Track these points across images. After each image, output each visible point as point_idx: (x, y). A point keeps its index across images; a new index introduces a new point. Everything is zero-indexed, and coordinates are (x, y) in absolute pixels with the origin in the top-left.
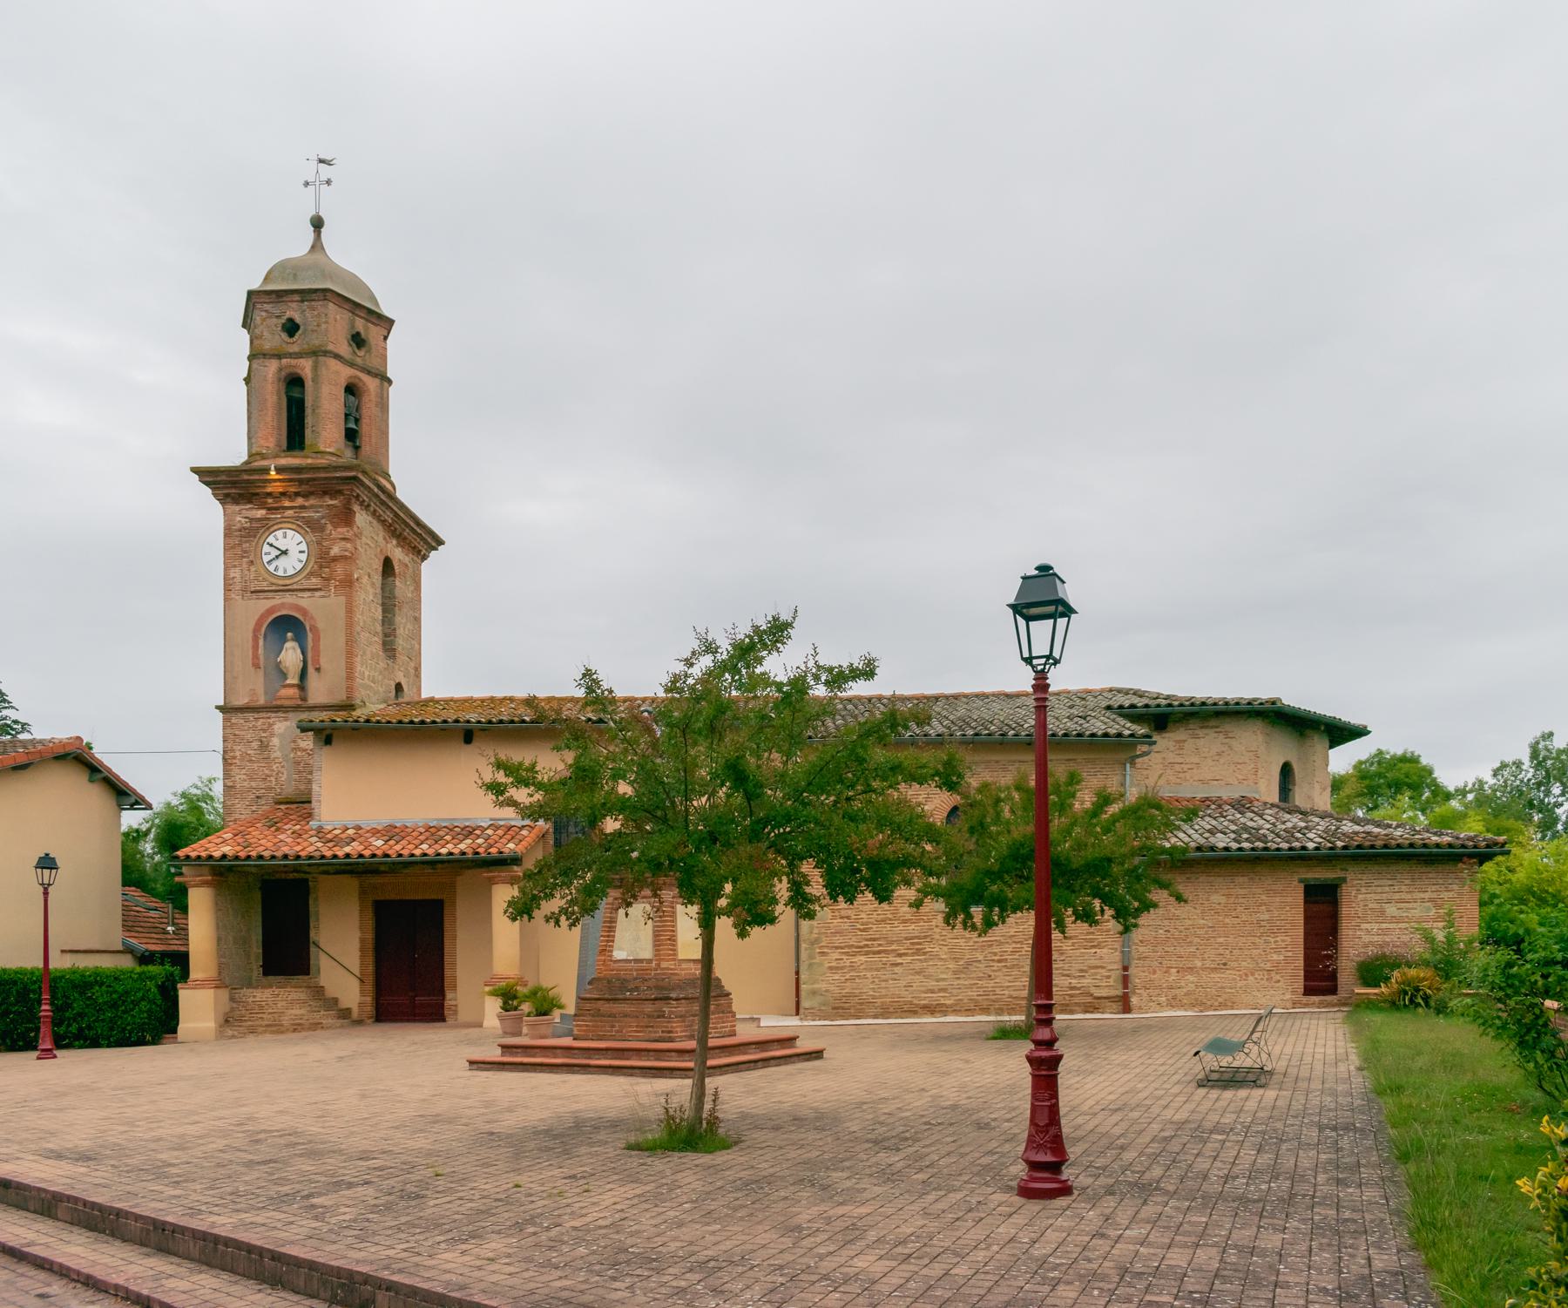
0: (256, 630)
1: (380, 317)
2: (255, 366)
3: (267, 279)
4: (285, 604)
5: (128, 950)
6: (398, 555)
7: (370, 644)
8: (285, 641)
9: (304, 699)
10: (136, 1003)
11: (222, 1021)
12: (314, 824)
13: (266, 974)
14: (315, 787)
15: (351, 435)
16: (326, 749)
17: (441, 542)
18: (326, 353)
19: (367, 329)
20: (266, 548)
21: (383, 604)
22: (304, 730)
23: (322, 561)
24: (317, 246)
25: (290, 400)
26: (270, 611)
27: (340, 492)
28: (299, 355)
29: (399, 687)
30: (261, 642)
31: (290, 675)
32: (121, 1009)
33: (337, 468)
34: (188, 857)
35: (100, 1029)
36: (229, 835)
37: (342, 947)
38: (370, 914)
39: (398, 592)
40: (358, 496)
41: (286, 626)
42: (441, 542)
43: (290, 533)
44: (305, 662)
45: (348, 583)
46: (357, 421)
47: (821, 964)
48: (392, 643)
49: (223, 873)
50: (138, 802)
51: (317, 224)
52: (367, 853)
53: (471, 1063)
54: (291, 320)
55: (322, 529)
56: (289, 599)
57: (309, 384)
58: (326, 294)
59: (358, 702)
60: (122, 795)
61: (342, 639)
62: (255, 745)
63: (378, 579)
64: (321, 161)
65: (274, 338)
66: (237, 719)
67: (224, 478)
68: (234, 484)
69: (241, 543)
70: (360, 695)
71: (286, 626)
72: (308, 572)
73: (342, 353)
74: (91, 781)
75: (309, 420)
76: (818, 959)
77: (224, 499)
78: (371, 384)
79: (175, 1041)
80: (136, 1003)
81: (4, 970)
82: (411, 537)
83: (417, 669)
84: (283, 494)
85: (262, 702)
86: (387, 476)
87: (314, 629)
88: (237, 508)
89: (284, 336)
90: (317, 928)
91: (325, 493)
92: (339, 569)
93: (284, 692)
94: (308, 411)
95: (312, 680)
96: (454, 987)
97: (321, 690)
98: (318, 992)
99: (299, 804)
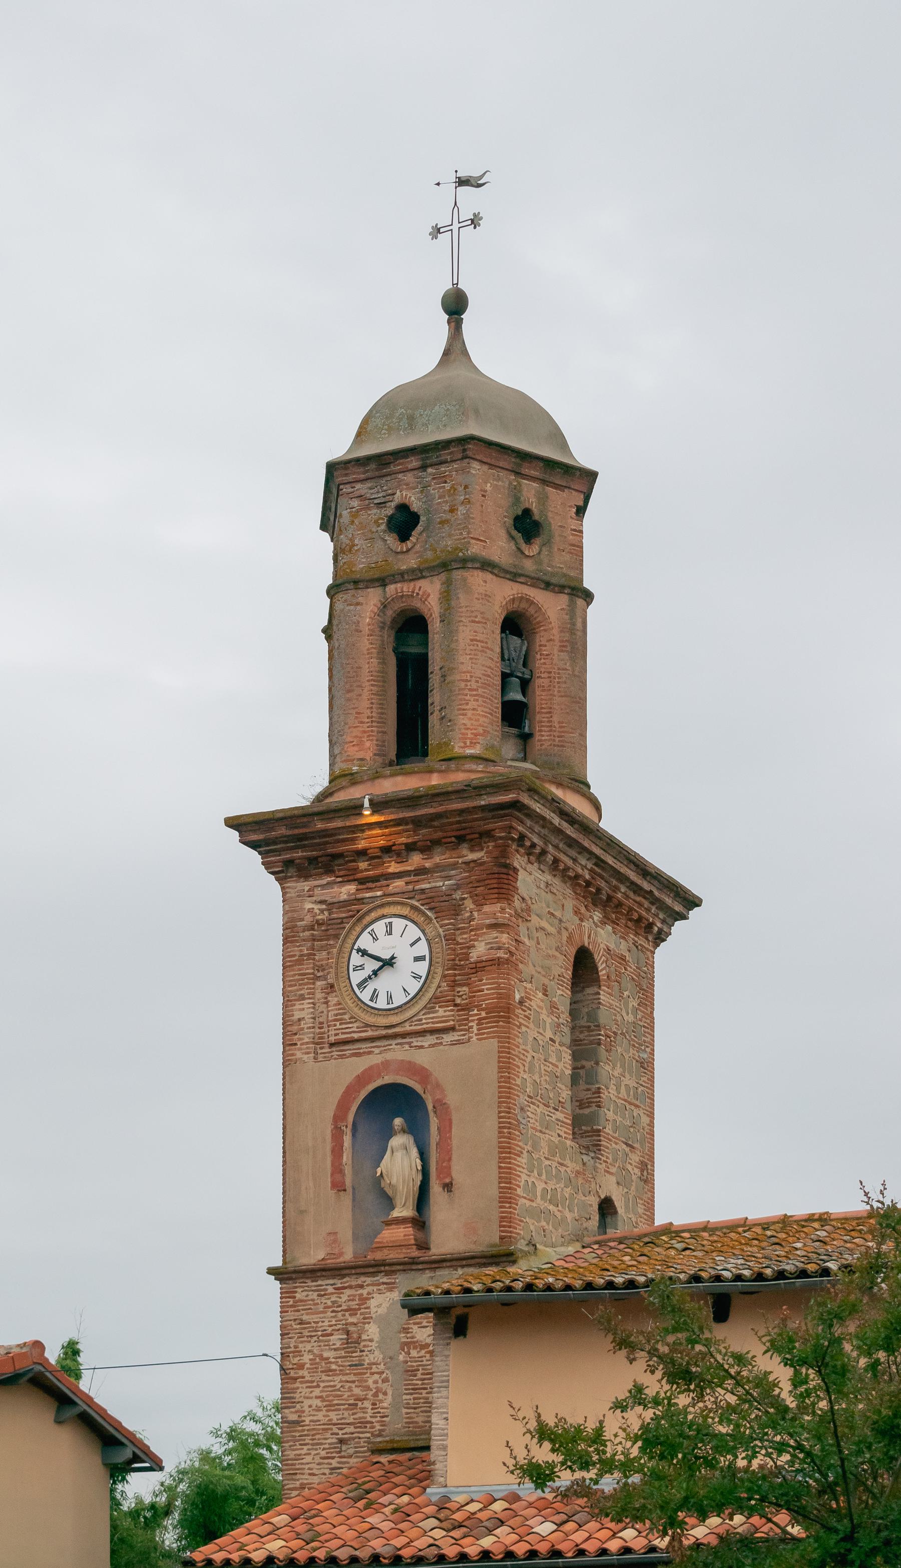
0: (339, 1117)
2: (339, 606)
3: (362, 434)
4: (388, 1062)
6: (604, 938)
7: (546, 1127)
8: (389, 1133)
9: (423, 1246)
12: (434, 1492)
14: (436, 1420)
15: (514, 715)
16: (457, 1344)
17: (692, 902)
18: (465, 563)
20: (356, 959)
21: (575, 1042)
22: (414, 1311)
23: (457, 973)
24: (455, 350)
26: (361, 1080)
27: (488, 834)
28: (417, 574)
29: (606, 1208)
30: (347, 1140)
31: (399, 1201)
33: (479, 789)
36: (281, 1520)
39: (603, 1016)
40: (522, 837)
41: (393, 1105)
42: (692, 902)
43: (399, 924)
44: (425, 1172)
45: (503, 1012)
46: (525, 684)
48: (592, 1119)
50: (142, 1458)
51: (455, 305)
52: (521, 1549)
54: (403, 508)
55: (456, 910)
56: (397, 1052)
57: (435, 626)
58: (465, 446)
59: (522, 1245)
60: (115, 1448)
61: (491, 1124)
62: (337, 1339)
63: (562, 995)
64: (462, 182)
65: (376, 548)
66: (304, 1292)
67: (282, 831)
68: (300, 840)
69: (313, 951)
70: (528, 1227)
71: (393, 1105)
72: (430, 997)
73: (495, 558)
74: (58, 1422)
75: (435, 698)
77: (284, 870)
78: (551, 606)
82: (630, 900)
85: (348, 1256)
86: (581, 785)
87: (442, 1107)
88: (305, 885)
89: (392, 540)
91: (461, 839)
92: (487, 986)
94: (434, 680)
97: (450, 1231)
99: (409, 1452)
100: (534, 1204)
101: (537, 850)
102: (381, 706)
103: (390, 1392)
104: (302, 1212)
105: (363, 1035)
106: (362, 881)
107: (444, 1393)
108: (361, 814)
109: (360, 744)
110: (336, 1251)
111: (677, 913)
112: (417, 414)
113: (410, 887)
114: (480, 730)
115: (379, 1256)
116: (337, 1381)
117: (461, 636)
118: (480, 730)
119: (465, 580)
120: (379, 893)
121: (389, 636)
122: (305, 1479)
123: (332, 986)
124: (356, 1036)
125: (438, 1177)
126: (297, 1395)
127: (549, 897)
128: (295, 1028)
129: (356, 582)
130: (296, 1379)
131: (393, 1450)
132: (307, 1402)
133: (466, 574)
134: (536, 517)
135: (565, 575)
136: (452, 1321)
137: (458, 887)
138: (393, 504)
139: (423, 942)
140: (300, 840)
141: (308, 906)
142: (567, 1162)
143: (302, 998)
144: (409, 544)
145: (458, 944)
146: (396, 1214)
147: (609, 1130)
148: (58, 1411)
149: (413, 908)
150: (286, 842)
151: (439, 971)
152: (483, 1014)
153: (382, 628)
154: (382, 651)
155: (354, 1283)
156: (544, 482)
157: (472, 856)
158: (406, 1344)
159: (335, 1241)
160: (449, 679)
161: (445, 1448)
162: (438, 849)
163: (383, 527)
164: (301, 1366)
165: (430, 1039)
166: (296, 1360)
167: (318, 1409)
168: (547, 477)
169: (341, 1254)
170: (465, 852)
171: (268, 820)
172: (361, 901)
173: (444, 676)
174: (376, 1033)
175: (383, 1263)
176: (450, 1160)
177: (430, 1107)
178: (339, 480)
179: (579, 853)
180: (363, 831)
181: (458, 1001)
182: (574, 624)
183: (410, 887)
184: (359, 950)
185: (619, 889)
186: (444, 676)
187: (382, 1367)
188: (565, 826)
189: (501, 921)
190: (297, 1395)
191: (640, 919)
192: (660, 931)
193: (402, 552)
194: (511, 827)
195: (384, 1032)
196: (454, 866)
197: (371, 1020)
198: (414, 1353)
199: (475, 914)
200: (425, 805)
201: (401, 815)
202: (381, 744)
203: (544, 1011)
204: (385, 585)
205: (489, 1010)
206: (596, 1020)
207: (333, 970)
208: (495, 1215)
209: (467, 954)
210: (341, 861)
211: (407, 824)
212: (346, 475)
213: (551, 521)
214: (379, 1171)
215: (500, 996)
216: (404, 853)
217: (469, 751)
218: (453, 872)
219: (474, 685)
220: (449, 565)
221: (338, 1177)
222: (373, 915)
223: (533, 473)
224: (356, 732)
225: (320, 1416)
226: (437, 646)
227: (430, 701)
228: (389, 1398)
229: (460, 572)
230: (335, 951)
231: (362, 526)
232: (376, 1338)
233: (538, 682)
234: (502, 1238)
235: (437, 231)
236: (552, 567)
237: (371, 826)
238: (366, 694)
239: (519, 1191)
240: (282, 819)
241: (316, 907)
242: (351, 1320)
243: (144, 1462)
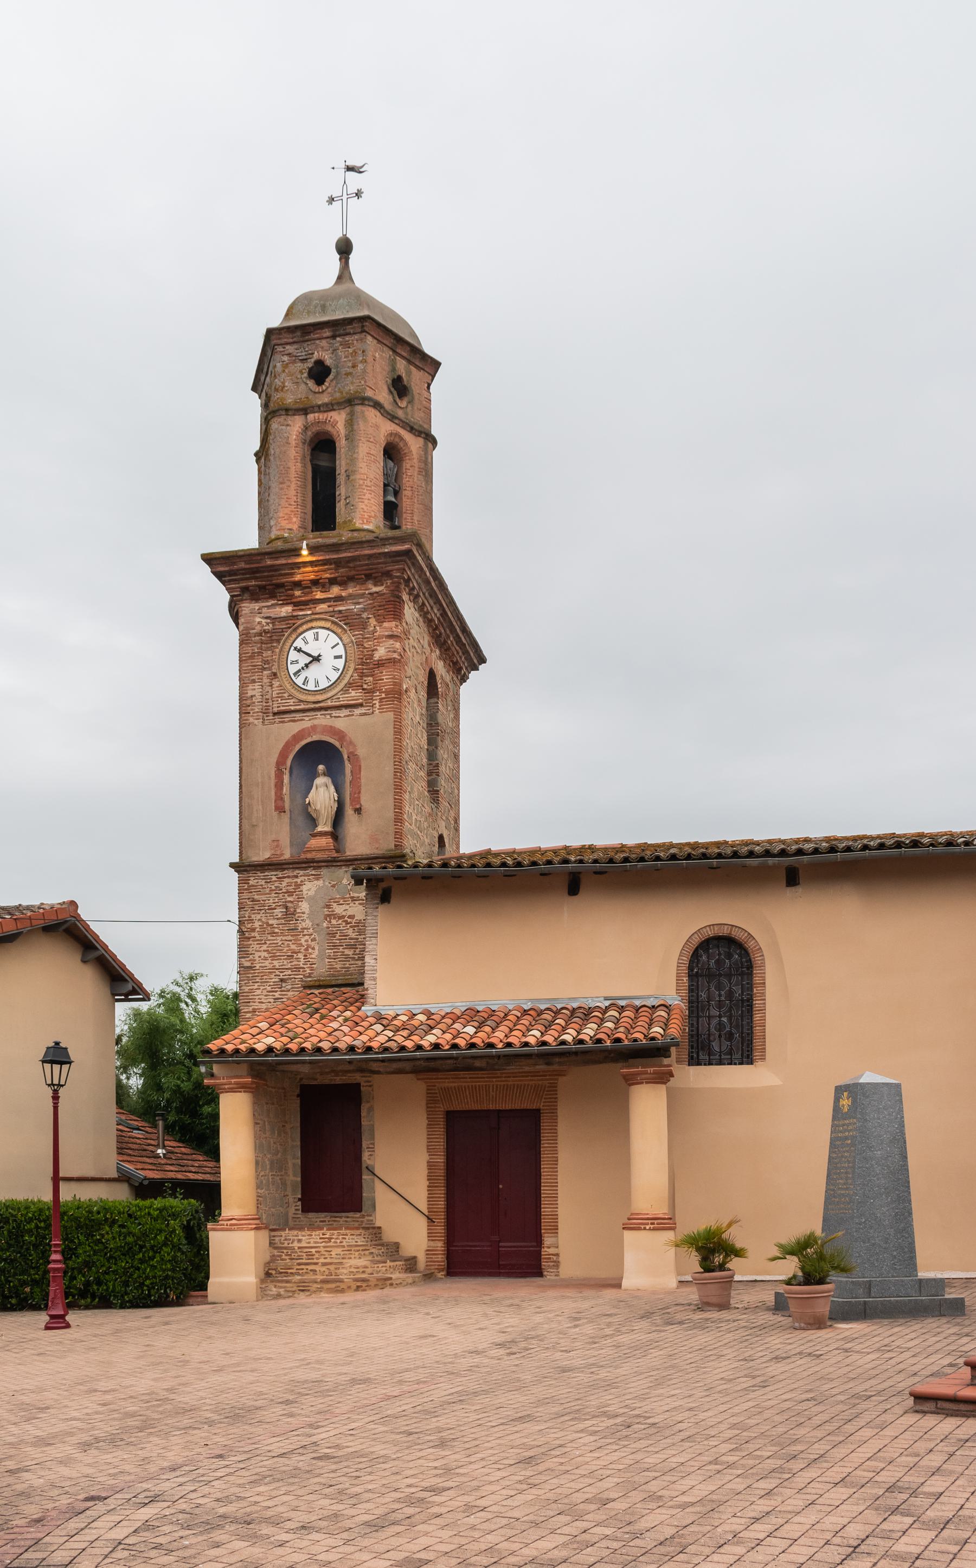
0: (280, 763)
1: (424, 357)
4: (316, 726)
5: (123, 1177)
8: (315, 775)
10: (156, 1249)
11: (262, 1275)
12: (367, 1009)
13: (306, 1209)
18: (364, 400)
19: (409, 373)
20: (293, 655)
23: (364, 668)
24: (344, 275)
25: (316, 471)
26: (297, 737)
27: (388, 574)
30: (286, 778)
32: (119, 1255)
34: (222, 1051)
35: (114, 1283)
36: (264, 1025)
37: (403, 1173)
38: (441, 1131)
41: (319, 756)
43: (323, 633)
45: (396, 694)
46: (396, 493)
49: (263, 1071)
51: (344, 248)
53: (919, 1398)
54: (320, 363)
55: (364, 625)
56: (321, 720)
57: (341, 444)
59: (407, 851)
60: (118, 980)
61: (389, 769)
62: (279, 912)
63: (423, 694)
64: (350, 169)
65: (295, 388)
67: (242, 565)
68: (253, 573)
69: (261, 653)
70: (409, 844)
71: (319, 756)
74: (84, 961)
75: (342, 491)
78: (414, 444)
79: (204, 1300)
80: (156, 1249)
81: (10, 1205)
83: (457, 820)
84: (315, 583)
85: (287, 855)
87: (353, 757)
88: (256, 606)
89: (311, 383)
90: (372, 1149)
91: (368, 577)
92: (386, 677)
93: (314, 843)
94: (341, 479)
95: (345, 824)
96: (555, 1229)
97: (361, 839)
98: (376, 1233)
99: (348, 986)
102: (304, 495)
103: (317, 948)
104: (254, 826)
106: (296, 604)
107: (374, 941)
108: (300, 555)
109: (289, 519)
110: (278, 852)
112: (328, 304)
113: (331, 609)
114: (373, 514)
115: (309, 856)
116: (279, 940)
117: (360, 449)
118: (373, 514)
119: (363, 412)
120: (309, 612)
122: (256, 1005)
123: (275, 674)
124: (292, 708)
125: (351, 804)
126: (250, 949)
128: (248, 702)
129: (287, 410)
130: (249, 938)
131: (319, 987)
132: (257, 954)
133: (365, 408)
135: (421, 426)
136: (380, 892)
137: (364, 610)
138: (313, 360)
139: (341, 646)
140: (254, 573)
141: (258, 620)
143: (254, 681)
144: (324, 387)
145: (365, 648)
146: (319, 829)
147: (442, 791)
148: (83, 955)
149: (333, 622)
151: (352, 666)
152: (383, 695)
153: (304, 443)
154: (304, 457)
155: (291, 874)
156: (409, 362)
157: (375, 589)
158: (329, 915)
159: (277, 846)
160: (352, 478)
161: (375, 979)
162: (352, 584)
163: (306, 375)
164: (253, 930)
165: (345, 712)
166: (249, 926)
167: (266, 959)
169: (282, 854)
170: (370, 586)
171: (233, 556)
172: (296, 617)
173: (348, 476)
174: (307, 707)
175: (313, 861)
176: (359, 792)
177: (345, 757)
178: (273, 342)
180: (299, 568)
181: (365, 686)
183: (331, 609)
184: (295, 648)
186: (348, 476)
187: (311, 931)
189: (395, 633)
190: (250, 949)
193: (319, 393)
194: (404, 569)
195: (313, 706)
196: (362, 596)
197: (303, 697)
198: (334, 922)
199: (378, 628)
200: (345, 551)
201: (327, 557)
202: (303, 520)
204: (306, 414)
205: (387, 693)
206: (436, 719)
207: (276, 664)
208: (392, 829)
209: (372, 655)
210: (281, 590)
211: (331, 564)
212: (280, 339)
214: (307, 800)
215: (395, 684)
216: (328, 585)
217: (366, 527)
218: (361, 600)
219: (369, 484)
220: (351, 402)
221: (280, 803)
222: (305, 627)
223: (403, 353)
224: (286, 511)
225: (267, 963)
226: (343, 456)
227: (337, 493)
228: (316, 952)
230: (277, 650)
231: (290, 374)
232: (307, 911)
233: (405, 493)
234: (396, 846)
235: (331, 200)
237: (305, 564)
238: (293, 486)
239: (405, 816)
240: (242, 556)
241: (264, 621)
242: (289, 899)
243: (139, 994)
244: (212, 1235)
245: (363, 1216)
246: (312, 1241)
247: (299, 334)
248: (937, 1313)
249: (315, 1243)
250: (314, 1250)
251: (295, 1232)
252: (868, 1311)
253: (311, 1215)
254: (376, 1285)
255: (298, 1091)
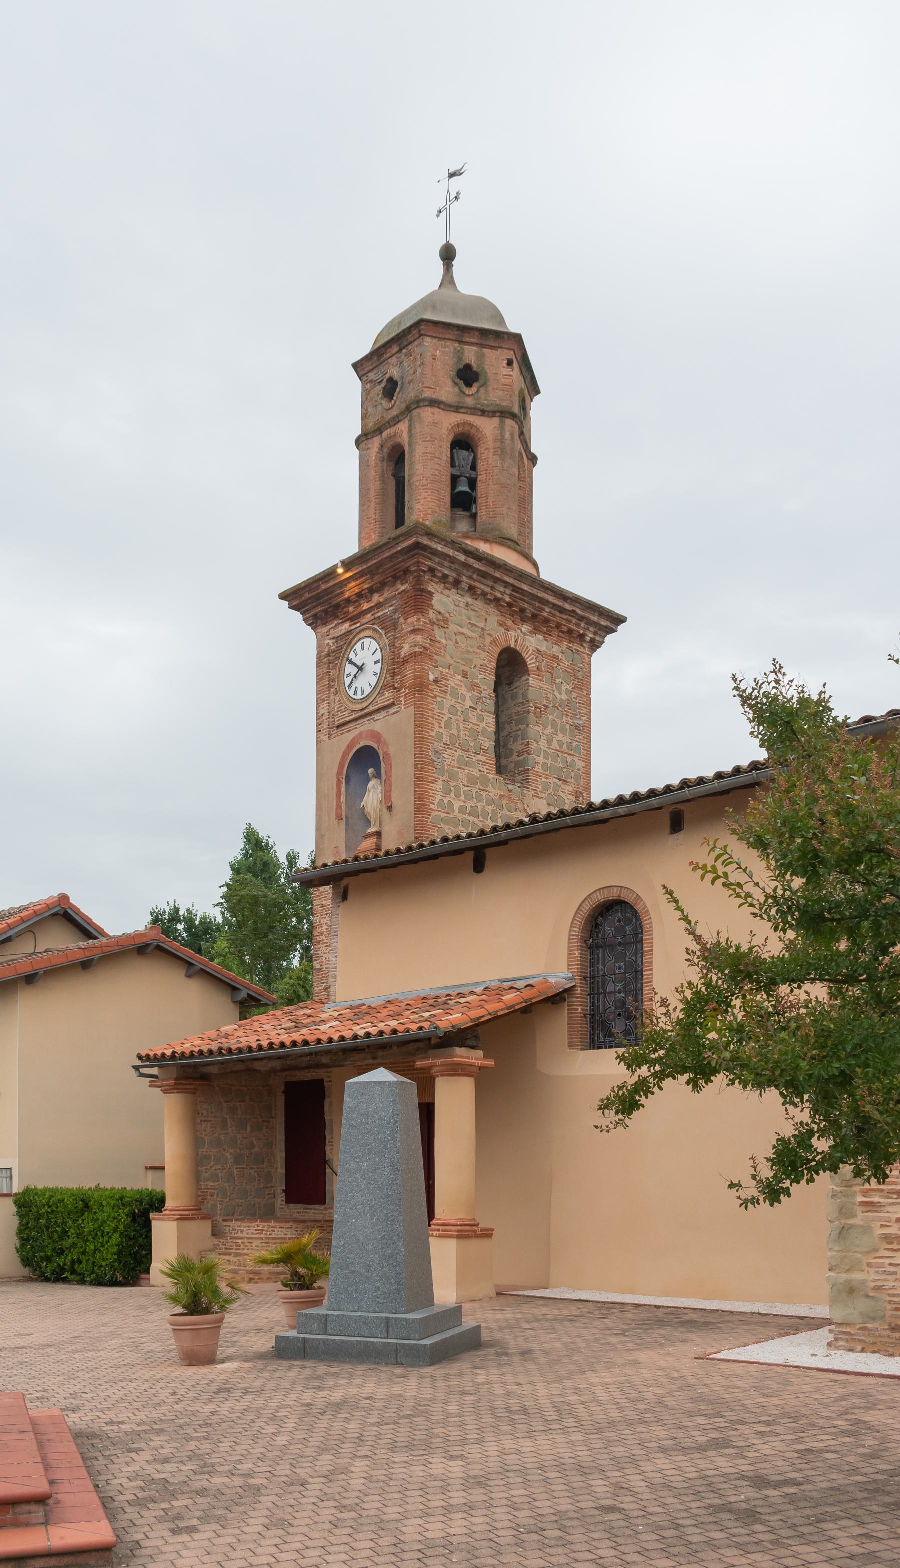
8: (368, 780)
24: (448, 279)
26: (350, 747)
27: (406, 572)
39: (532, 694)
43: (367, 641)
46: (473, 483)
47: (867, 1229)
51: (448, 254)
56: (366, 726)
64: (452, 175)
72: (383, 686)
74: (189, 976)
76: (860, 1218)
77: (314, 621)
84: (360, 595)
87: (387, 754)
91: (396, 578)
100: (451, 816)
101: (451, 580)
105: (351, 718)
111: (606, 627)
118: (430, 511)
119: (419, 415)
121: (388, 466)
124: (347, 719)
127: (472, 613)
132: (325, 956)
134: (475, 369)
135: (498, 405)
140: (318, 599)
141: (327, 642)
142: (490, 788)
144: (393, 402)
150: (312, 603)
156: (481, 346)
161: (335, 976)
165: (383, 713)
168: (484, 342)
177: (382, 758)
179: (495, 582)
180: (346, 585)
182: (503, 436)
185: (544, 610)
188: (472, 561)
189: (417, 627)
191: (570, 631)
192: (593, 641)
194: (418, 562)
195: (360, 714)
197: (354, 707)
203: (464, 688)
204: (381, 433)
205: (410, 688)
213: (488, 371)
216: (369, 595)
219: (425, 482)
222: (356, 639)
223: (473, 340)
229: (416, 411)
236: (488, 400)
238: (373, 505)
240: (305, 587)
244: (155, 1224)
245: (326, 1209)
246: (250, 1231)
247: (375, 359)
248: (393, 1360)
249: (252, 1233)
250: (240, 1241)
251: (239, 1223)
252: (308, 1350)
253: (292, 1206)
254: (268, 1278)
255: (283, 1088)
